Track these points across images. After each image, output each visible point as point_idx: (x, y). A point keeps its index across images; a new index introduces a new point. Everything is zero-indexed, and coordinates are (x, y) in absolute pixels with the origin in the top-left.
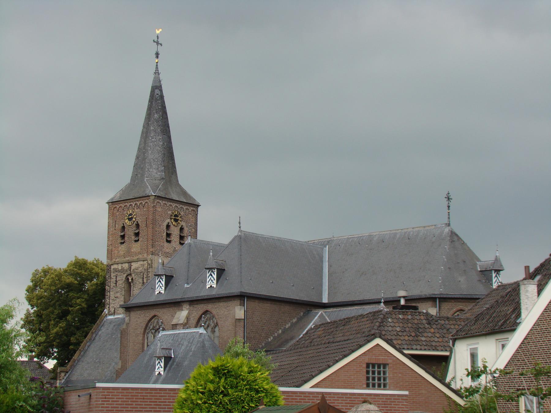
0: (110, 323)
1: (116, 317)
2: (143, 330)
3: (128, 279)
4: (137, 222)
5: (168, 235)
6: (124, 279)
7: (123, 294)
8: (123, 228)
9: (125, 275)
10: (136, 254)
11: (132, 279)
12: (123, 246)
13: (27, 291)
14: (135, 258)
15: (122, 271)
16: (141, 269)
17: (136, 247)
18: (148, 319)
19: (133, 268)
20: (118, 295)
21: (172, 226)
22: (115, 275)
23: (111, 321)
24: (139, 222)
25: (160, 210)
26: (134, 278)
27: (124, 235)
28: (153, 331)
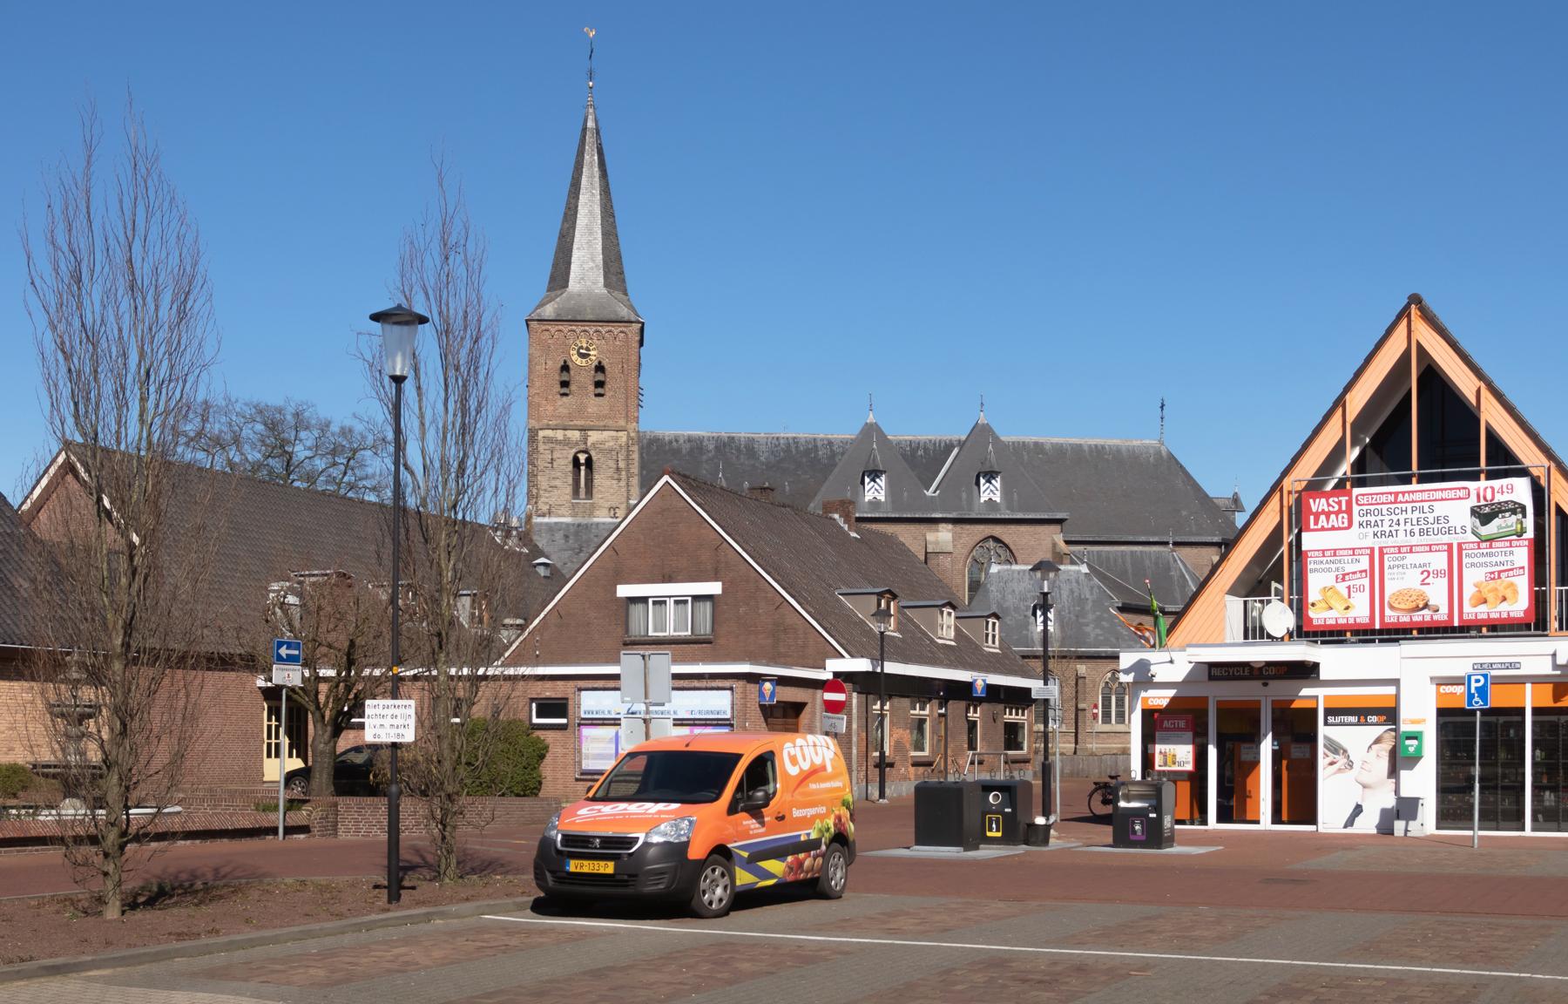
10: (599, 418)
12: (565, 399)
15: (566, 442)
20: (557, 483)
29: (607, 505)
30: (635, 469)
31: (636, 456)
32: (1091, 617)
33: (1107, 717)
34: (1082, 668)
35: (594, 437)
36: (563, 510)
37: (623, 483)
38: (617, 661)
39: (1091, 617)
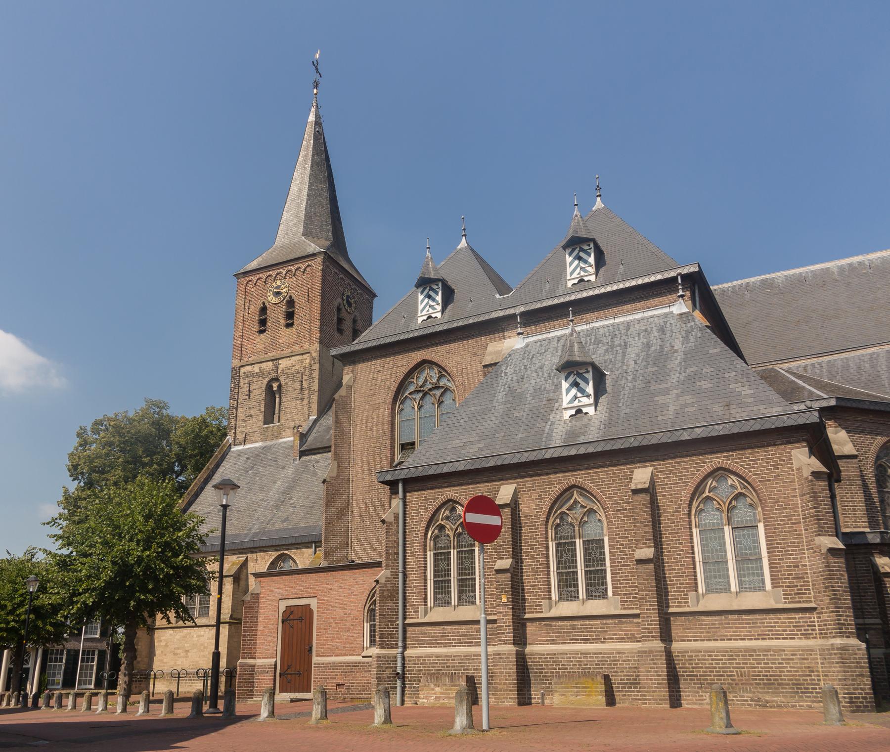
0: (239, 456)
1: (248, 446)
2: (391, 395)
3: (272, 387)
4: (290, 297)
5: (340, 321)
6: (264, 386)
7: (263, 410)
8: (264, 310)
9: (267, 380)
10: (288, 346)
11: (280, 386)
12: (262, 336)
13: (74, 471)
14: (287, 352)
15: (261, 374)
16: (297, 367)
17: (286, 336)
18: (405, 370)
19: (281, 367)
20: (253, 412)
21: (344, 310)
22: (246, 381)
23: (240, 453)
24: (294, 297)
25: (330, 279)
26: (283, 383)
27: (266, 319)
28: (418, 397)
29: (292, 425)
30: (315, 387)
31: (316, 374)
32: (675, 377)
33: (568, 585)
34: (641, 475)
35: (283, 364)
36: (257, 436)
37: (305, 402)
38: (775, 585)
39: (675, 377)
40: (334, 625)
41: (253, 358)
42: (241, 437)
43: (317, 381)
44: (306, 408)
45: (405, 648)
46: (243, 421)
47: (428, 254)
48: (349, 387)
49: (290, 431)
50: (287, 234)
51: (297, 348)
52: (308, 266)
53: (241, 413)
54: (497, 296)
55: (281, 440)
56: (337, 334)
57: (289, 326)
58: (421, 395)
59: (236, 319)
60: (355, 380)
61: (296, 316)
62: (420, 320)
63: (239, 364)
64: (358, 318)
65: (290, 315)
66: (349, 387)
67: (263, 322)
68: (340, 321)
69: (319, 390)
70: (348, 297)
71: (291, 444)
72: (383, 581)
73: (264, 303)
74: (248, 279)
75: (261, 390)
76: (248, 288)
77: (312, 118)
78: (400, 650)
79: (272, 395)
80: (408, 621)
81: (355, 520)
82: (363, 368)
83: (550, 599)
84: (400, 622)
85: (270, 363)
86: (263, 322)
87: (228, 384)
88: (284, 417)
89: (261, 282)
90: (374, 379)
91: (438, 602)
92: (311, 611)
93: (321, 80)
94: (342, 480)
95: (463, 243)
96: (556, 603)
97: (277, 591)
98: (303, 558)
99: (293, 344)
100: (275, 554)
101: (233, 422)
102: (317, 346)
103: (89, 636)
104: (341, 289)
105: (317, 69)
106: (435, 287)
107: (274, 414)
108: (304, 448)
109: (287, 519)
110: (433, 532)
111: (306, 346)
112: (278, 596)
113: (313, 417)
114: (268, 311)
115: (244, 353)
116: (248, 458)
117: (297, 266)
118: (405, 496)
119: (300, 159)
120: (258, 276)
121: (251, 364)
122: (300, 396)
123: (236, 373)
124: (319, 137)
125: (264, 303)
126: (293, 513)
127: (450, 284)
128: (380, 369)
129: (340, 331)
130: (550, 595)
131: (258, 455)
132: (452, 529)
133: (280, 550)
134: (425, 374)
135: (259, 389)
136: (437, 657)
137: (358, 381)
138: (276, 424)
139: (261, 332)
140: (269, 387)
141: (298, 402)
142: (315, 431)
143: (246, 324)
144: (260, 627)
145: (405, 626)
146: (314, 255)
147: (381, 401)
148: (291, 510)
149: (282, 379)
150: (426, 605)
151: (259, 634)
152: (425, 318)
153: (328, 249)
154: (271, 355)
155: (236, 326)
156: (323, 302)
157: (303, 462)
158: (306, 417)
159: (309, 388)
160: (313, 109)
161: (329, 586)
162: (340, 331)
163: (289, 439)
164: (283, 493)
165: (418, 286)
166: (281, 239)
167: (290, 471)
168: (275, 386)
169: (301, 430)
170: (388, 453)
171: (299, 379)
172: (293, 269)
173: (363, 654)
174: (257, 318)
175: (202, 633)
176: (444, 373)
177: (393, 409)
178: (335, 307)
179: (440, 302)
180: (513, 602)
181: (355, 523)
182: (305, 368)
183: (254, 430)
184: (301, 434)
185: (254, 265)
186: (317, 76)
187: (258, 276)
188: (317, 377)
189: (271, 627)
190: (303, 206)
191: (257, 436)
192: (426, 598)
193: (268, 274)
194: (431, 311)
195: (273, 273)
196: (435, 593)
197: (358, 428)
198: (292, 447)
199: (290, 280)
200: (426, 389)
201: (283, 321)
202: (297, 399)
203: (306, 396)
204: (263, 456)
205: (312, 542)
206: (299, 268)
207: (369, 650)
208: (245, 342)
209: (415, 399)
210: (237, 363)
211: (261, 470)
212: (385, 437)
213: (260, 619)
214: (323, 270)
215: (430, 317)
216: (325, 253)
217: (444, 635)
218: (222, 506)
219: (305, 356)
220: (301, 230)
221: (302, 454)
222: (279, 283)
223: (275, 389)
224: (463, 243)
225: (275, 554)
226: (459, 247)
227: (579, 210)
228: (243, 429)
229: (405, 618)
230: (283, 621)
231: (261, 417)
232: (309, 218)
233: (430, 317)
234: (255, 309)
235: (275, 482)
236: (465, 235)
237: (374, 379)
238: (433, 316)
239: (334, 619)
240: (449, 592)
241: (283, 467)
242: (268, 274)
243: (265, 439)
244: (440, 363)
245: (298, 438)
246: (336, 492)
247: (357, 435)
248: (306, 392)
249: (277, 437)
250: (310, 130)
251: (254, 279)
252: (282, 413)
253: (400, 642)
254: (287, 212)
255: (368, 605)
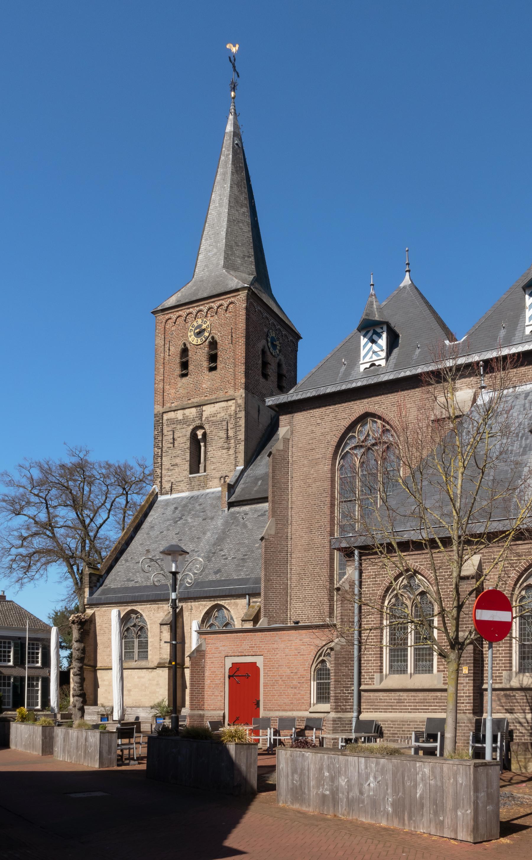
1: (174, 496)
2: (331, 450)
3: (196, 435)
4: (213, 338)
5: (265, 364)
6: (188, 434)
7: (188, 458)
8: (185, 351)
9: (191, 427)
11: (204, 435)
12: (185, 380)
15: (185, 421)
16: (223, 414)
18: (346, 423)
22: (170, 429)
23: (167, 503)
24: (217, 338)
26: (208, 432)
29: (218, 475)
30: (242, 436)
31: (242, 422)
35: (208, 410)
37: (232, 451)
40: (280, 682)
41: (175, 404)
42: (167, 486)
43: (243, 430)
44: (232, 457)
45: (360, 712)
46: (168, 469)
47: (372, 292)
48: (286, 441)
49: (216, 481)
50: (206, 266)
51: (221, 395)
52: (231, 303)
53: (166, 461)
54: (447, 342)
55: (208, 491)
56: (262, 380)
57: (212, 369)
58: (363, 450)
59: (156, 361)
60: (292, 433)
61: (219, 359)
62: (362, 368)
63: (161, 410)
64: (283, 363)
65: (213, 358)
66: (286, 441)
67: (185, 365)
68: (265, 364)
69: (246, 439)
70: (272, 338)
71: (218, 495)
72: (338, 648)
73: (185, 344)
74: (167, 317)
75: (185, 439)
76: (167, 327)
77: (229, 128)
78: (355, 714)
79: (197, 444)
80: (362, 687)
81: (294, 578)
82: (300, 417)
83: (511, 670)
84: (355, 688)
85: (194, 410)
86: (185, 365)
87: (151, 432)
88: (209, 467)
89: (181, 320)
90: (312, 432)
91: (393, 670)
92: (258, 669)
93: (239, 81)
94: (281, 537)
95: (407, 281)
96: (516, 674)
97: (223, 648)
98: (237, 610)
99: (217, 389)
100: (209, 604)
101: (159, 471)
102: (242, 392)
103: (32, 665)
104: (266, 330)
105: (234, 67)
106: (379, 330)
107: (199, 462)
108: (233, 499)
109: (218, 571)
110: (390, 601)
111: (231, 392)
112: (224, 654)
113: (240, 468)
114: (190, 353)
115: (166, 398)
116: (176, 508)
117: (218, 303)
118: (361, 564)
119: (218, 178)
120: (178, 314)
121: (174, 411)
122: (226, 445)
123: (159, 419)
124: (239, 153)
125: (185, 344)
126: (226, 565)
127: (392, 325)
128: (319, 421)
129: (265, 376)
130: (511, 667)
131: (185, 506)
132: (410, 598)
133: (214, 601)
134: (367, 427)
135: (183, 436)
136: (392, 721)
137: (295, 434)
138: (202, 473)
139: (184, 375)
140: (193, 435)
141: (225, 451)
142: (242, 481)
143: (167, 368)
144: (207, 682)
145: (360, 691)
146: (237, 290)
147: (320, 456)
148: (223, 561)
149: (206, 426)
150: (381, 672)
151: (206, 687)
152: (368, 365)
153: (252, 284)
154: (196, 400)
155: (156, 369)
156: (247, 344)
157: (233, 513)
158: (232, 467)
159: (236, 436)
160: (231, 117)
161: (275, 646)
162: (265, 376)
163: (216, 488)
164: (214, 544)
165: (360, 329)
166: (201, 271)
167: (219, 522)
168: (200, 433)
169: (228, 480)
170: (328, 512)
171: (225, 427)
172: (215, 306)
173: (311, 710)
174: (178, 360)
175: (143, 675)
176: (388, 427)
177: (333, 465)
178: (260, 349)
179: (385, 347)
180: (474, 673)
181: (293, 580)
182: (230, 415)
183: (180, 479)
184: (229, 484)
185: (172, 301)
186: (234, 75)
187: (178, 314)
188: (243, 425)
189: (218, 682)
190: (223, 234)
191: (183, 486)
192: (381, 666)
193: (188, 311)
194: (375, 358)
195: (194, 311)
196: (391, 661)
197: (296, 484)
198: (220, 498)
199: (212, 319)
200: (369, 443)
201: (205, 364)
202: (223, 448)
203: (232, 445)
204: (190, 506)
205: (247, 594)
206: (221, 305)
207: (316, 706)
208: (167, 387)
209: (356, 455)
210: (159, 409)
211: (190, 520)
212: (325, 495)
213: (207, 673)
214: (247, 308)
215: (373, 365)
216: (249, 289)
217: (400, 701)
218: (172, 572)
219: (230, 403)
220: (222, 263)
221: (231, 505)
222: (200, 321)
223: (200, 437)
224: (407, 281)
225: (209, 604)
226: (402, 285)
227: (373, 289)
228: (169, 479)
229: (360, 684)
230: (230, 677)
231: (187, 466)
232: (229, 248)
233: (373, 365)
234: (175, 350)
235: (204, 533)
236: (409, 271)
237: (312, 432)
238: (377, 363)
239: (281, 676)
240: (406, 661)
241: (212, 518)
242: (188, 311)
243: (192, 489)
244: (384, 416)
245: (226, 489)
246: (275, 550)
247: (295, 491)
248: (232, 441)
249: (205, 487)
250: (228, 142)
251: (174, 316)
252: (208, 463)
253: (355, 707)
254: (206, 240)
255: (314, 665)
